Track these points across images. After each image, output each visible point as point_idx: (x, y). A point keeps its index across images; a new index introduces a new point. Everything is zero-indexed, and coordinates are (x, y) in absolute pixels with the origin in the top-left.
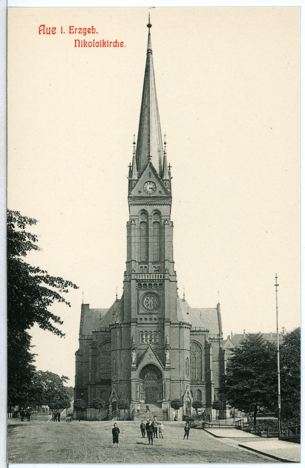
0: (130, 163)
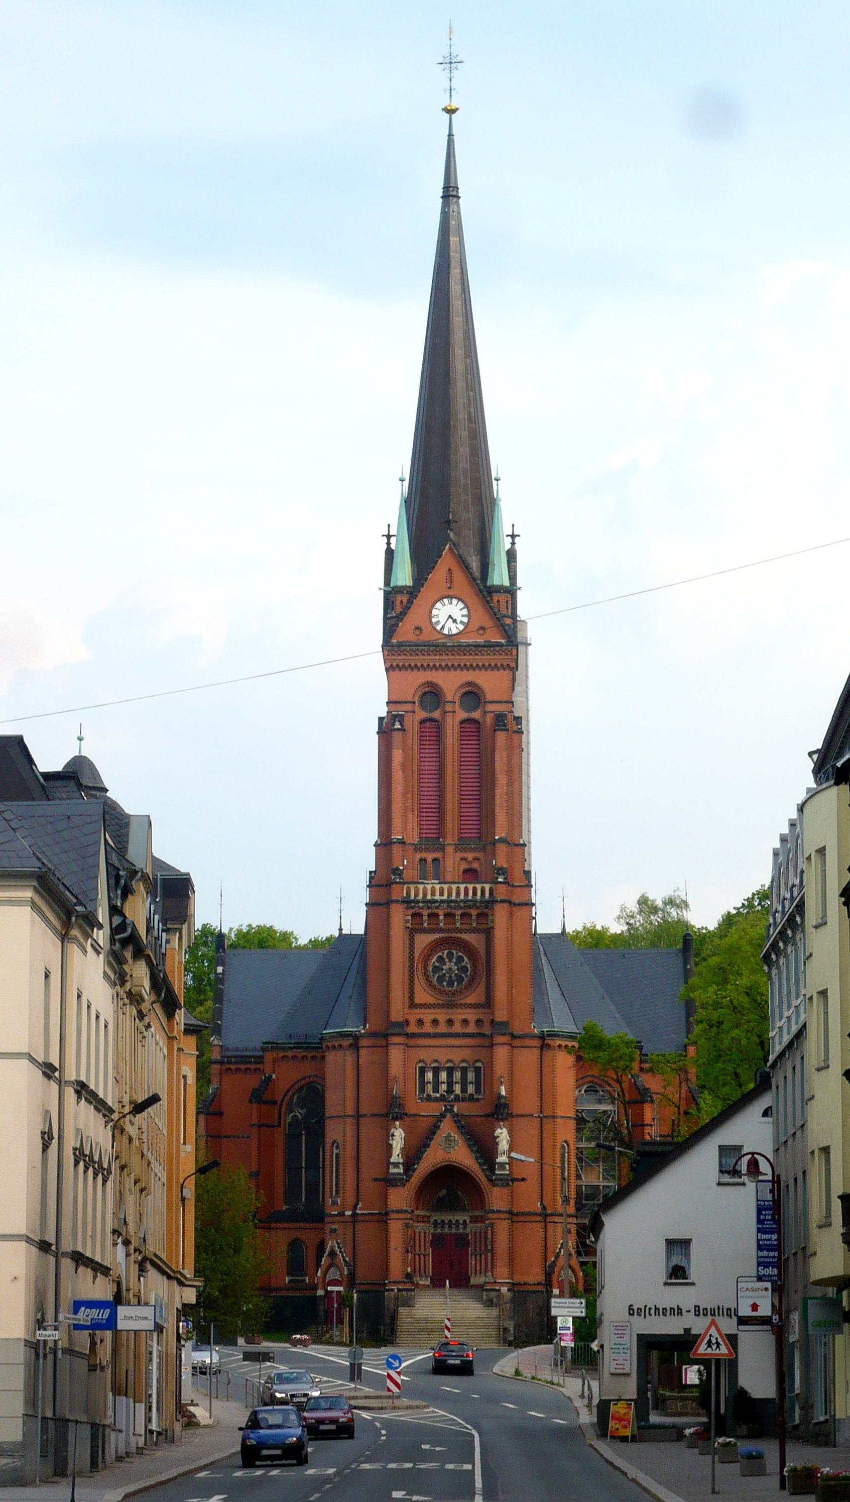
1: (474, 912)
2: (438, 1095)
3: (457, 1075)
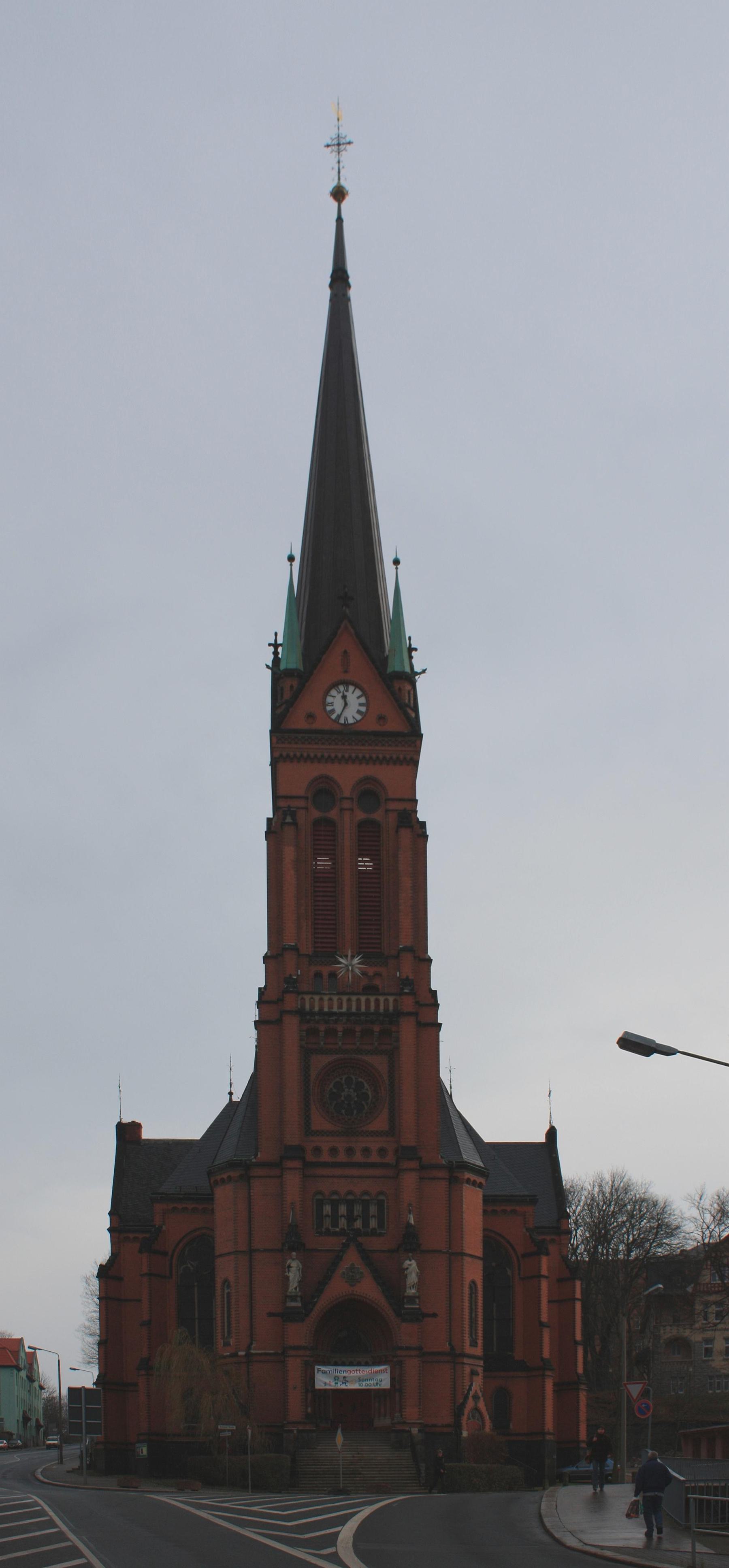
0: (276, 634)
1: (376, 1028)
2: (337, 1230)
3: (358, 1209)
